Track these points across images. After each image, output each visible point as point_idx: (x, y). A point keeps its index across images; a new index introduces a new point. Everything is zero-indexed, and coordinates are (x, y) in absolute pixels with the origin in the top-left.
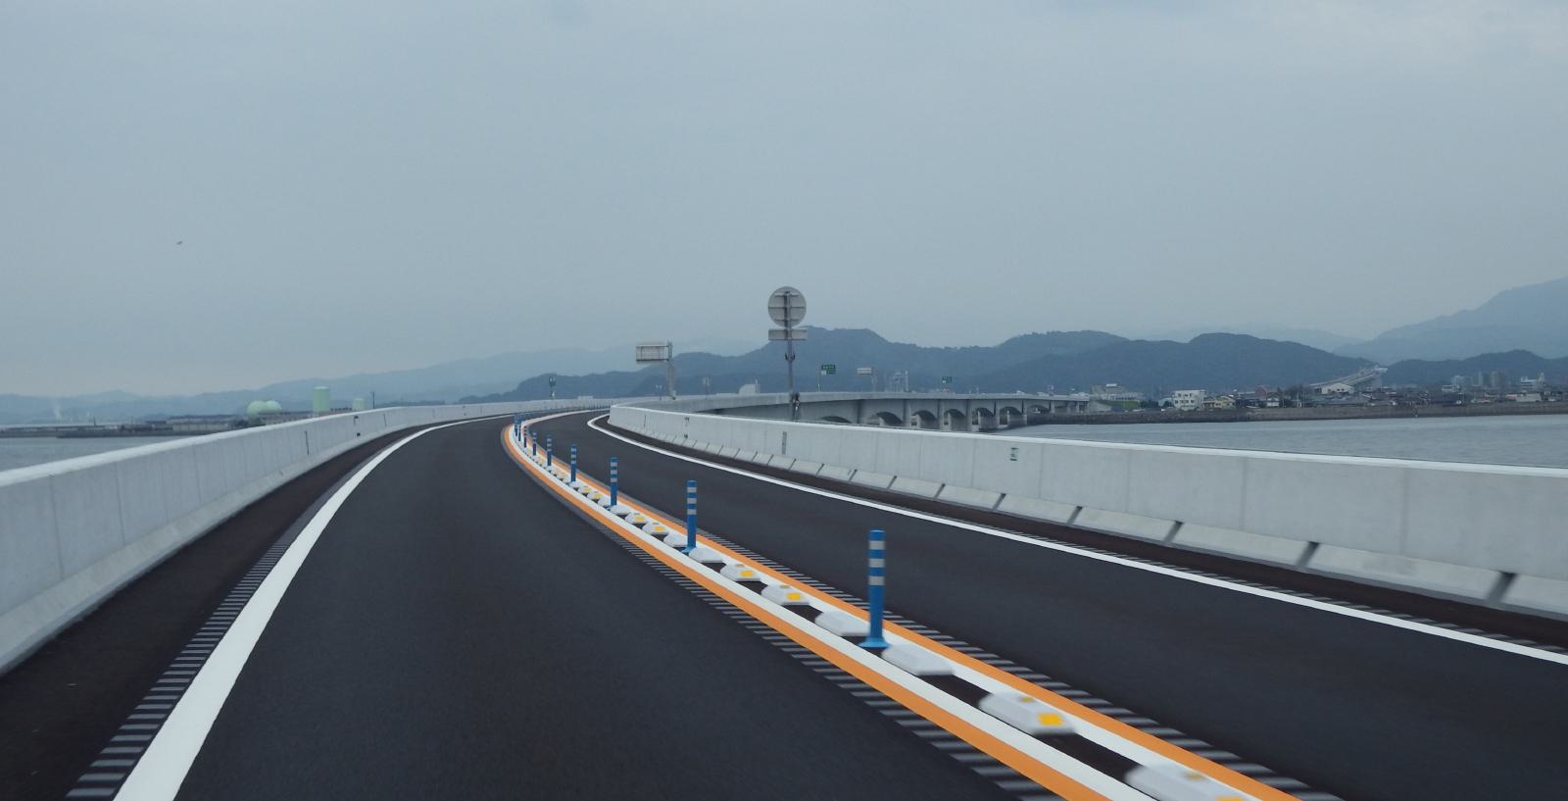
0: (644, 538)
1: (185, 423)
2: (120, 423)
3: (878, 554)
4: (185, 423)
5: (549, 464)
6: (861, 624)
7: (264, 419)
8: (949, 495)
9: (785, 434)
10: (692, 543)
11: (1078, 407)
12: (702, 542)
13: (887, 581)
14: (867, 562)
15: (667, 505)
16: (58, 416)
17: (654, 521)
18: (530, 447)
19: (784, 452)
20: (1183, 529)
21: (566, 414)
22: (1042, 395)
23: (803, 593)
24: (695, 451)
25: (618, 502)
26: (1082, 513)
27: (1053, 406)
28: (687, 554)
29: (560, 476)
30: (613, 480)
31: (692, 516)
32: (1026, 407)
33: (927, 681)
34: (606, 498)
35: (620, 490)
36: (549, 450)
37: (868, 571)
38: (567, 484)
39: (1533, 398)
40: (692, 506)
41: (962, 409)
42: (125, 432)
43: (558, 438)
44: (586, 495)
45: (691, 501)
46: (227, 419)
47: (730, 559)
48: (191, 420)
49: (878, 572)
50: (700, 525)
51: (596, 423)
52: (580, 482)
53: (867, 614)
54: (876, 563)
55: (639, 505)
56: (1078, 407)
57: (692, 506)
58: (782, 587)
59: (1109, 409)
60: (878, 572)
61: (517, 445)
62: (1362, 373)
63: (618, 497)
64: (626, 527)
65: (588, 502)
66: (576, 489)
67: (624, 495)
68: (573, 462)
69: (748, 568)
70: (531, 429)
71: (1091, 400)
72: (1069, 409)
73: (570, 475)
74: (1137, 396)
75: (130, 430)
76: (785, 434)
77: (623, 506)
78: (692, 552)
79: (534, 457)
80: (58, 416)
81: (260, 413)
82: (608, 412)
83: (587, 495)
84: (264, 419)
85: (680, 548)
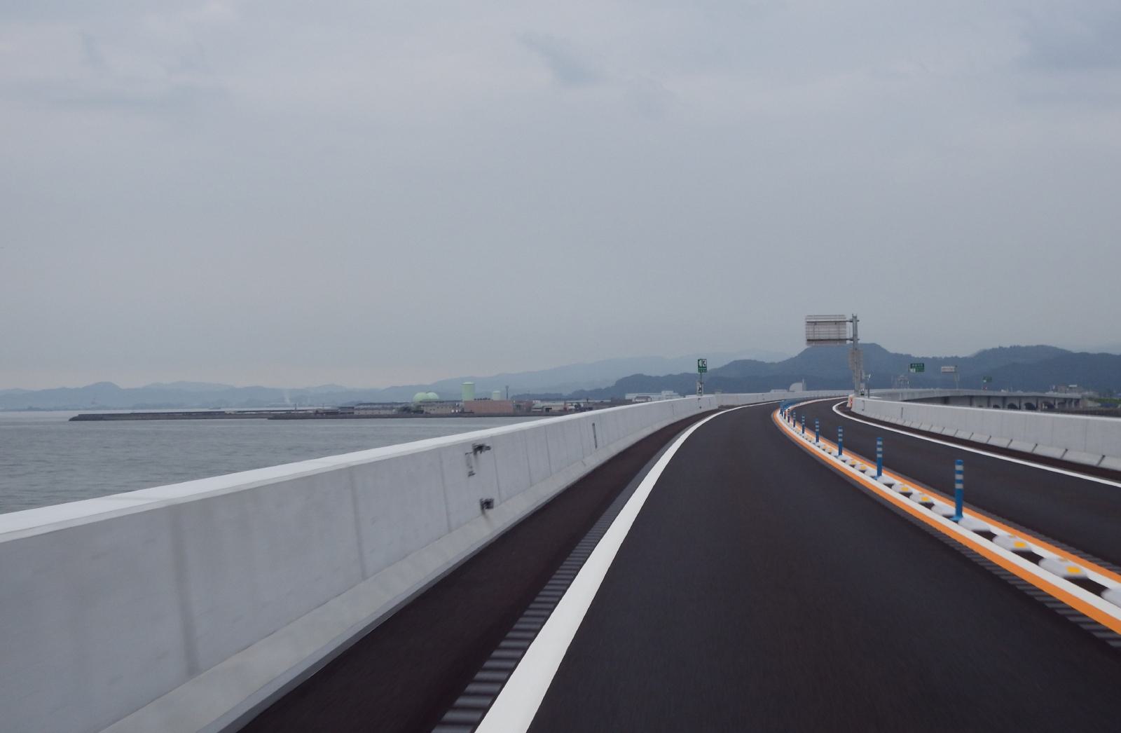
0: (855, 473)
1: (363, 409)
2: (315, 408)
3: (960, 472)
4: (363, 409)
5: (803, 432)
6: (951, 509)
7: (423, 406)
8: (1071, 457)
9: (902, 409)
10: (959, 513)
11: (1073, 403)
12: (967, 512)
13: (964, 486)
14: (876, 449)
15: (866, 453)
16: (288, 401)
17: (860, 463)
18: (791, 423)
19: (902, 417)
20: (1106, 458)
21: (825, 400)
22: (1050, 394)
23: (1082, 567)
24: (911, 428)
25: (883, 474)
26: (1013, 442)
27: (1057, 403)
28: (956, 522)
29: (809, 439)
30: (840, 440)
31: (960, 490)
32: (1039, 403)
33: (983, 536)
34: (836, 451)
35: (821, 435)
36: (803, 424)
37: (954, 481)
38: (814, 444)
39: (609, 401)
40: (880, 453)
41: (1052, 402)
42: (318, 415)
43: (806, 416)
44: (824, 450)
45: (959, 477)
46: (397, 406)
47: (915, 490)
48: (385, 406)
49: (960, 482)
50: (968, 499)
51: (838, 408)
52: (821, 442)
53: (954, 503)
54: (879, 449)
55: (928, 489)
56: (1073, 403)
57: (880, 453)
58: (1010, 537)
59: (1099, 404)
60: (960, 482)
61: (778, 416)
62: (572, 405)
63: (883, 470)
64: (846, 467)
65: (825, 454)
66: (819, 447)
67: (967, 504)
68: (817, 430)
69: (906, 485)
70: (791, 413)
71: (1083, 398)
72: (1067, 405)
73: (815, 439)
74: (600, 401)
75: (322, 414)
76: (902, 409)
77: (845, 456)
78: (961, 522)
79: (803, 435)
80: (288, 401)
81: (421, 402)
82: (847, 399)
83: (826, 451)
84: (423, 406)
85: (873, 477)
